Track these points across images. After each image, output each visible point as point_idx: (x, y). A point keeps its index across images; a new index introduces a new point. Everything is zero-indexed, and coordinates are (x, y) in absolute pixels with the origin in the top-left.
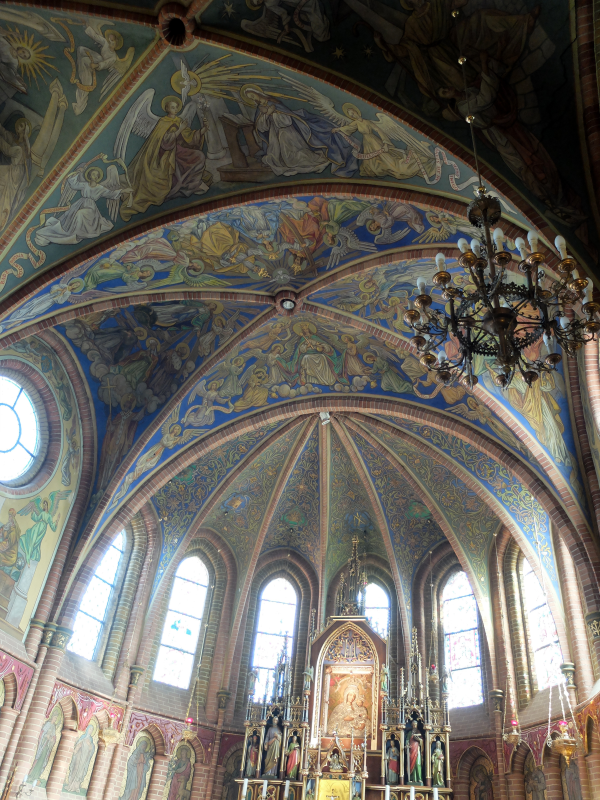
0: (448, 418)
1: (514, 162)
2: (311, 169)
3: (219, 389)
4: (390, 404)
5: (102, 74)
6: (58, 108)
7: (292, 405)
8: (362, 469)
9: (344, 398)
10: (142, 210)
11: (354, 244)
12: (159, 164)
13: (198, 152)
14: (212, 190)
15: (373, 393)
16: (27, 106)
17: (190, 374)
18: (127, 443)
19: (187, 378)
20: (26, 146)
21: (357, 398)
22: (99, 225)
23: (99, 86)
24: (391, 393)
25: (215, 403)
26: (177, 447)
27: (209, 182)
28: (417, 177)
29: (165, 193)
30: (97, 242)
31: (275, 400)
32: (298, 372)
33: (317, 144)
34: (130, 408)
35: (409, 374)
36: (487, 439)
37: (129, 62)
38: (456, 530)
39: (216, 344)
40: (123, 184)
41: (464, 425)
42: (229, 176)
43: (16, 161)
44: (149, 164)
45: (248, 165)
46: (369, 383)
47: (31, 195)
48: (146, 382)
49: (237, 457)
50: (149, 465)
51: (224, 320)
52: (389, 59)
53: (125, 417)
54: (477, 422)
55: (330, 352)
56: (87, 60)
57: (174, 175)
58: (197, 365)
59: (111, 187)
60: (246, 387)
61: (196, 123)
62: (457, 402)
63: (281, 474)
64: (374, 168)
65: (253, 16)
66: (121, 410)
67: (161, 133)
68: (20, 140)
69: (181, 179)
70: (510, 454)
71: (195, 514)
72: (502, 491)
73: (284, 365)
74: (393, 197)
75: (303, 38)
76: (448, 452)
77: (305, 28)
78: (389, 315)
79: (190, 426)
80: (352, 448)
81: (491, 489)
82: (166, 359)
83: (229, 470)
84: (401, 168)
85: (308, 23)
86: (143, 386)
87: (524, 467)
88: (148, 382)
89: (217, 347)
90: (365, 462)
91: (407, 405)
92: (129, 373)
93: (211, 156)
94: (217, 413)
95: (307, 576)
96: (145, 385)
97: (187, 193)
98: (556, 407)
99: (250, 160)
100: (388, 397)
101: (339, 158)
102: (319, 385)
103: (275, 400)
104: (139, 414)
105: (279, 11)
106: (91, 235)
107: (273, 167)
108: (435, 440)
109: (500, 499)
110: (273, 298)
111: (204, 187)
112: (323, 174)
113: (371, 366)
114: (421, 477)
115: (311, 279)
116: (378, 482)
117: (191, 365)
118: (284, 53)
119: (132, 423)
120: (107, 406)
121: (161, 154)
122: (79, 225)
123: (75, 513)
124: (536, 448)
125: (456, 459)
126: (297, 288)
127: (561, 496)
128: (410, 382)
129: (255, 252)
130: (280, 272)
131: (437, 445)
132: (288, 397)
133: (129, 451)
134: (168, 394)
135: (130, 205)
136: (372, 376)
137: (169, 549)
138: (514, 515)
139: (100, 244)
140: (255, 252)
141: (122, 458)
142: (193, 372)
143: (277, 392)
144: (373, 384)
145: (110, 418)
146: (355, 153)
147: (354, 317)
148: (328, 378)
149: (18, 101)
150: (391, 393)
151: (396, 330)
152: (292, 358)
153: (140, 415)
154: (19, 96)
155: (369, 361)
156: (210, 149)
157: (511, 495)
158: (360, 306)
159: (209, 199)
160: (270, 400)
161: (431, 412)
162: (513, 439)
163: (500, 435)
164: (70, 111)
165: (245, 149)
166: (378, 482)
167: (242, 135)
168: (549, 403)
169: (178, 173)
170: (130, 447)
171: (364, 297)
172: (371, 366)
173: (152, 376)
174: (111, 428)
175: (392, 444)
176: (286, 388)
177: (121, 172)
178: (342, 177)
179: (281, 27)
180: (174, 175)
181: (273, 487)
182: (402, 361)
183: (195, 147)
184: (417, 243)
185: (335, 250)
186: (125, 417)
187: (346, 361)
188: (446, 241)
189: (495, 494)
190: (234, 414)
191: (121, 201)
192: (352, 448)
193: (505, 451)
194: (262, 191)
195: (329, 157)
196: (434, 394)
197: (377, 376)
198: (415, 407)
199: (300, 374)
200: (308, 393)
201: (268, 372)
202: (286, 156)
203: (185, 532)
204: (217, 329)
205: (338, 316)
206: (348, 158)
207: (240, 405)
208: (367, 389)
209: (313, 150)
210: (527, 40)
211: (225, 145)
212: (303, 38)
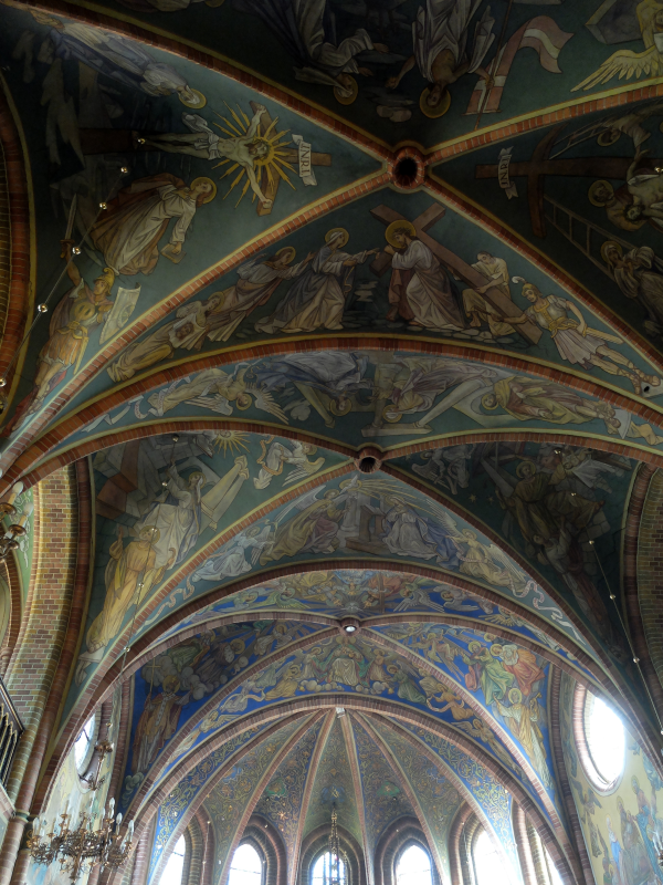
0: (453, 731)
1: (584, 605)
2: (421, 556)
3: (257, 681)
4: (404, 711)
5: (289, 467)
6: (238, 476)
7: (317, 698)
8: (352, 752)
9: (363, 699)
10: (276, 558)
11: (424, 601)
12: (302, 527)
13: (334, 524)
14: (337, 552)
15: (389, 699)
16: (207, 465)
17: (242, 669)
18: (169, 726)
19: (238, 673)
20: (196, 494)
21: (375, 701)
22: (241, 567)
23: (285, 474)
24: (405, 701)
25: (251, 692)
26: (211, 730)
27: (336, 547)
28: (506, 588)
29: (298, 548)
30: (235, 581)
31: (301, 693)
32: (328, 671)
33: (429, 540)
34: (173, 690)
35: (425, 689)
36: (486, 755)
37: (318, 468)
38: (426, 814)
39: (272, 647)
40: (270, 538)
41: (467, 739)
42: (354, 546)
43: (185, 505)
44: (295, 526)
45: (370, 540)
46: (387, 689)
47: (204, 545)
48: (193, 667)
49: (306, 761)
50: (186, 749)
51: (285, 629)
52: (503, 507)
53: (166, 699)
54: (478, 739)
55: (360, 659)
56: (279, 453)
57: (310, 537)
58: (251, 662)
59: (260, 540)
60: (279, 680)
61: (343, 506)
62: (464, 720)
63: (280, 752)
64: (471, 570)
65: (422, 463)
66: (162, 690)
67: (313, 509)
68: (191, 487)
69: (314, 540)
70: (505, 772)
71: (199, 788)
72: (477, 788)
73: (317, 664)
74: (486, 597)
75: (451, 484)
76: (437, 751)
77: (454, 477)
78: (426, 646)
79: (226, 712)
80: (350, 736)
81: (468, 786)
82: (218, 650)
83: (237, 747)
84: (495, 577)
85: (456, 475)
86: (188, 671)
87: (517, 785)
88: (195, 668)
89: (273, 649)
90: (357, 747)
91: (418, 714)
92: (176, 656)
93: (343, 528)
94: (250, 700)
95: (274, 844)
96: (192, 671)
97: (316, 551)
98: (540, 735)
99: (373, 538)
100: (402, 705)
101: (445, 554)
102: (343, 685)
103: (301, 693)
104: (184, 698)
105: (439, 463)
106: (232, 575)
107: (390, 546)
108: (427, 739)
109: (475, 796)
110: (340, 622)
111: (331, 549)
112: (428, 562)
113: (392, 676)
114: (403, 766)
115: (376, 614)
116: (363, 764)
117: (244, 661)
118: (438, 492)
119: (174, 708)
120: (149, 684)
121: (306, 521)
122: (226, 566)
123: (113, 787)
124: (532, 775)
125: (442, 757)
126: (362, 617)
127: (550, 818)
128: (425, 695)
129: (339, 588)
130: (352, 604)
131: (428, 743)
132: (313, 692)
133: (173, 736)
134: (217, 684)
135: (269, 553)
136: (391, 684)
137: (166, 822)
138: (485, 811)
139: (239, 582)
140: (339, 588)
141: (164, 744)
142: (245, 668)
143: (305, 687)
144: (391, 691)
145: (149, 696)
146: (458, 555)
147: (399, 644)
148: (352, 680)
149: (201, 460)
150: (405, 701)
151: (429, 659)
152: (325, 660)
153: (184, 700)
154: (203, 457)
155: (392, 672)
156: (345, 523)
157: (483, 793)
158: (404, 636)
159: (332, 559)
160: (298, 692)
161: (440, 724)
162: (511, 761)
163: (499, 755)
164: (248, 484)
165: (372, 531)
166: (363, 764)
167: (374, 519)
168: (535, 731)
169: (314, 535)
170: (174, 732)
171: (410, 630)
172: (392, 676)
173: (200, 663)
174: (150, 707)
175: (386, 735)
176: (314, 683)
177: (273, 530)
178: (444, 569)
179: (438, 473)
180: (310, 537)
181: (268, 762)
182: (422, 678)
183: (334, 520)
184: (483, 619)
185: (407, 600)
186: (166, 699)
187: (371, 668)
188: (509, 627)
189: (472, 792)
190: (264, 703)
191: (264, 550)
192: (350, 736)
193: (501, 768)
194: (378, 562)
195: (436, 551)
196: (444, 709)
197: (396, 686)
198: (426, 717)
199: (329, 674)
200: (332, 690)
201: (302, 669)
202: (402, 541)
203: (186, 806)
204: (277, 634)
205: (387, 643)
206: (452, 556)
207: (271, 695)
208: (385, 694)
209: (425, 543)
210: (593, 517)
211: (358, 523)
212: (451, 484)
